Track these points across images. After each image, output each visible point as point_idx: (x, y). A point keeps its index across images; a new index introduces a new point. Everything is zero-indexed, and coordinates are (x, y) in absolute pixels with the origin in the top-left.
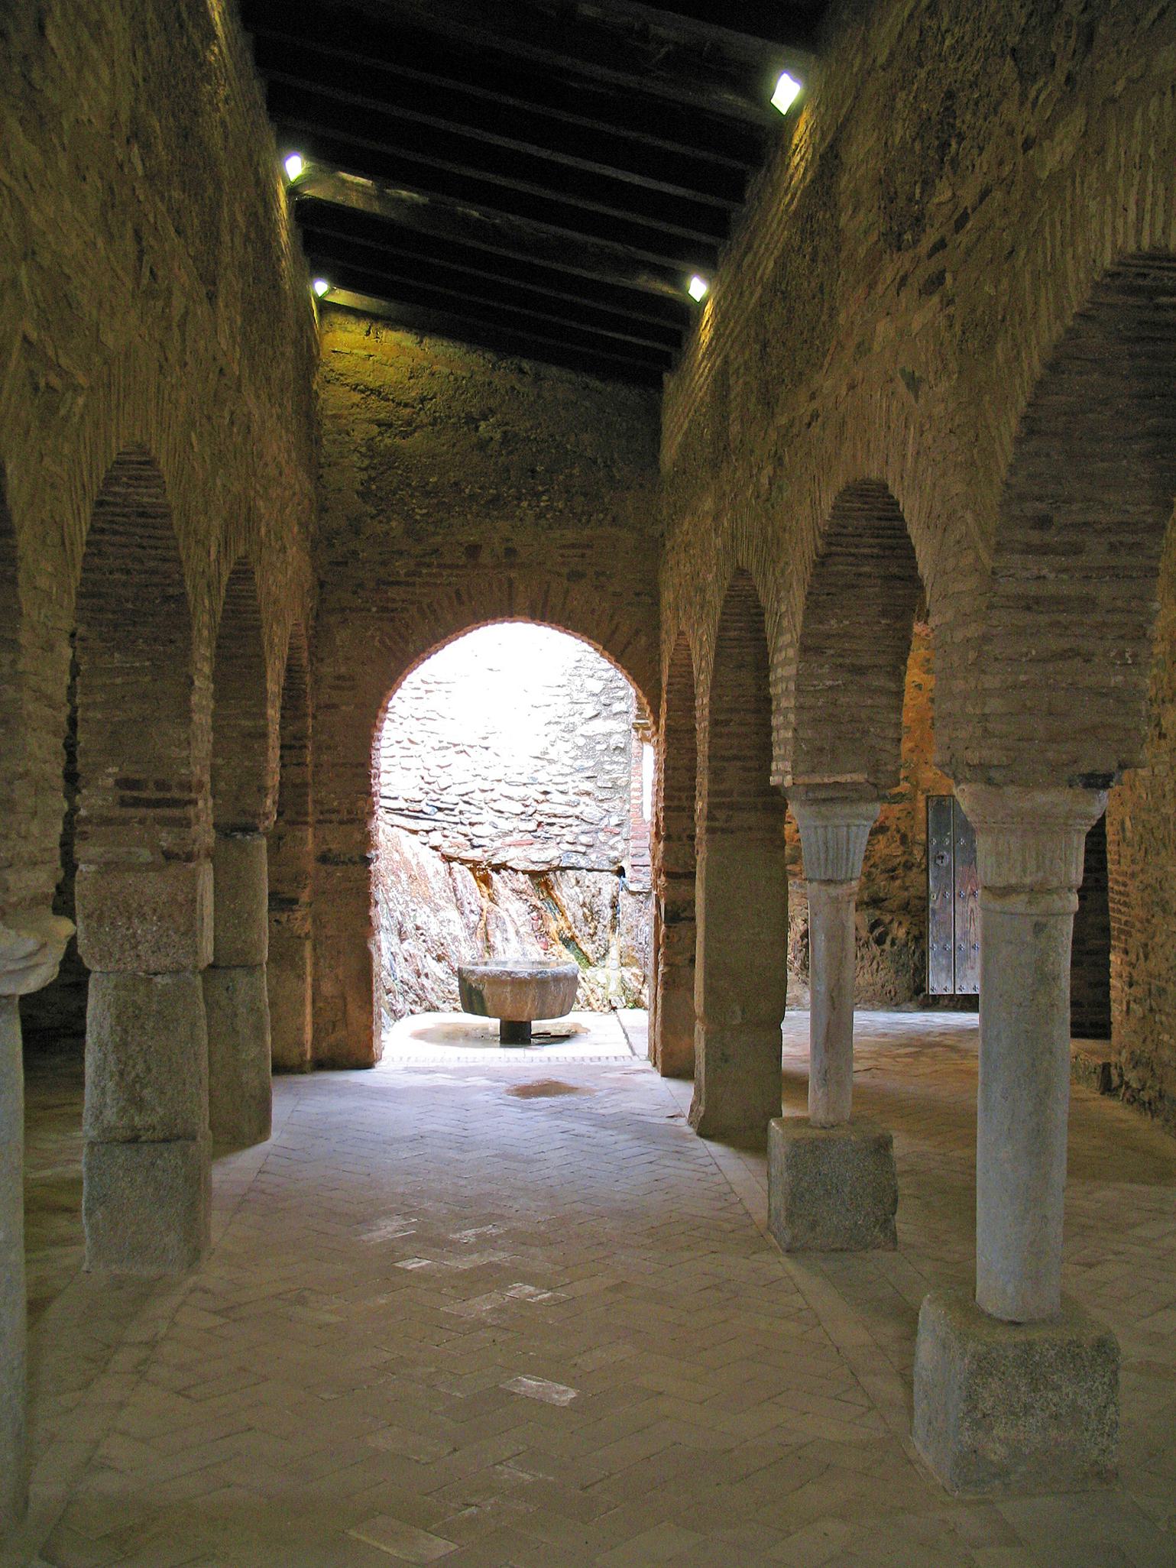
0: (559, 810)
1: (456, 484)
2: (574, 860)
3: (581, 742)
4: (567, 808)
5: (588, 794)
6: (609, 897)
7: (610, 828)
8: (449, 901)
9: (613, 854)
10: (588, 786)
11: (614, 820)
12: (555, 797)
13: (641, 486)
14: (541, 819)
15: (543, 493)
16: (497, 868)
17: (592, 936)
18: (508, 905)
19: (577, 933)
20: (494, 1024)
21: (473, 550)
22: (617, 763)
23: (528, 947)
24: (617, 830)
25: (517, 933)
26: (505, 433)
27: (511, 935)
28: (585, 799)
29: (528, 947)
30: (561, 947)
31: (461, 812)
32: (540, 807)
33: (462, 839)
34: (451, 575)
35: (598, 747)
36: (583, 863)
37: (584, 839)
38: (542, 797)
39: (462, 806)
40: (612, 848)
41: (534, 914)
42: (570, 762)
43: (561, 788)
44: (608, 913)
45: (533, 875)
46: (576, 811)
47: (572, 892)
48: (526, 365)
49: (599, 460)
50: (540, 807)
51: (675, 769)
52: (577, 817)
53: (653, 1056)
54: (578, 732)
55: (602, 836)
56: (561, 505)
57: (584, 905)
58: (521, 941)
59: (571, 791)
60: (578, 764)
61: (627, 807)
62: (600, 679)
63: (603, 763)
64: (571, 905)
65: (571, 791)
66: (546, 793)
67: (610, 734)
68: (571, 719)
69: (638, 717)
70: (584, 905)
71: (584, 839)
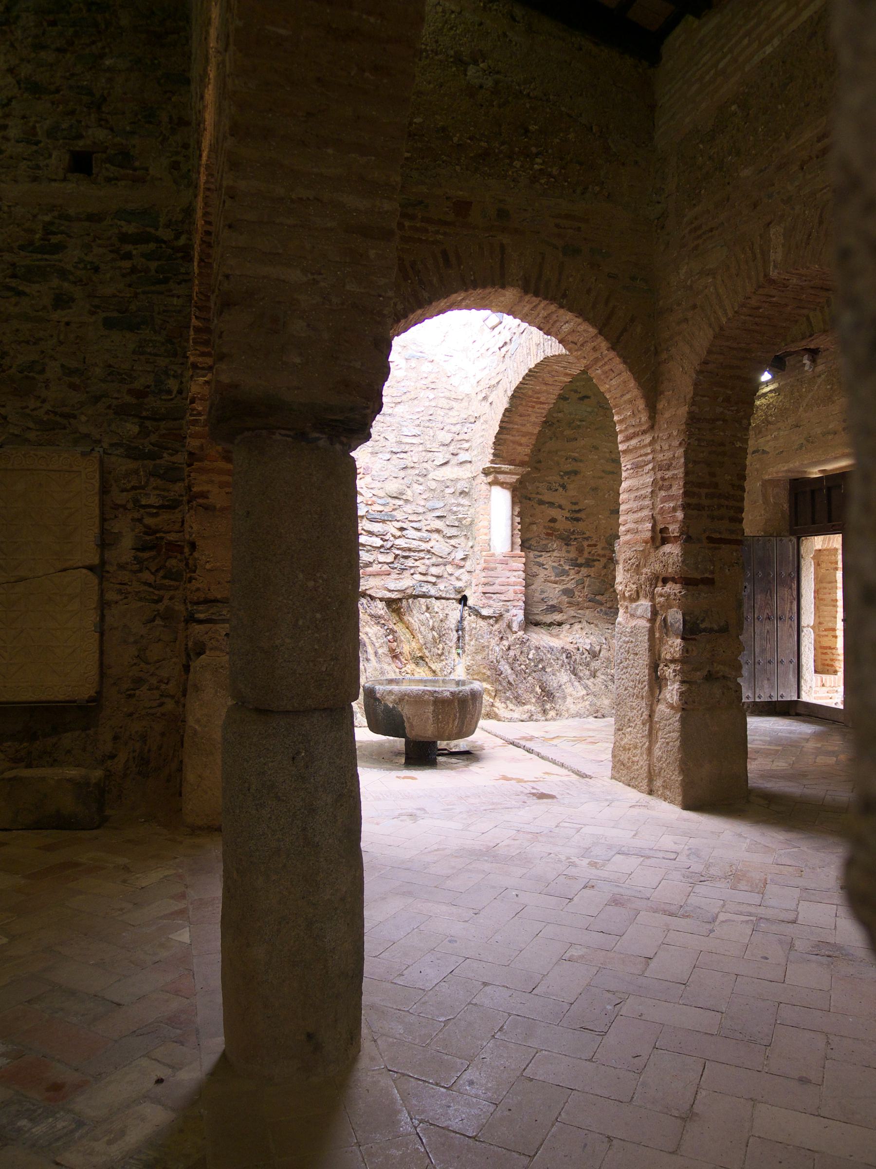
0: (414, 544)
1: (444, 129)
2: (425, 589)
4: (420, 543)
5: (438, 531)
6: (454, 622)
7: (456, 561)
9: (459, 584)
10: (439, 524)
11: (460, 555)
12: (411, 533)
13: (636, 162)
14: (397, 552)
15: (537, 155)
17: (440, 655)
18: (367, 629)
19: (427, 654)
20: (399, 743)
21: (462, 207)
23: (386, 666)
24: (462, 563)
25: (376, 653)
26: (497, 83)
28: (435, 536)
29: (386, 666)
30: (413, 666)
34: (437, 232)
35: (448, 491)
36: (433, 591)
37: (434, 570)
38: (398, 533)
40: (458, 579)
41: (390, 637)
42: (422, 503)
43: (415, 525)
44: (454, 635)
47: (422, 617)
48: (518, 12)
49: (595, 129)
51: (695, 462)
52: (429, 551)
53: (621, 768)
54: (430, 476)
55: (450, 569)
56: (555, 171)
57: (433, 629)
58: (379, 661)
60: (430, 504)
62: (449, 431)
64: (422, 628)
66: (402, 529)
67: (458, 480)
69: (492, 462)
70: (433, 629)
71: (434, 570)
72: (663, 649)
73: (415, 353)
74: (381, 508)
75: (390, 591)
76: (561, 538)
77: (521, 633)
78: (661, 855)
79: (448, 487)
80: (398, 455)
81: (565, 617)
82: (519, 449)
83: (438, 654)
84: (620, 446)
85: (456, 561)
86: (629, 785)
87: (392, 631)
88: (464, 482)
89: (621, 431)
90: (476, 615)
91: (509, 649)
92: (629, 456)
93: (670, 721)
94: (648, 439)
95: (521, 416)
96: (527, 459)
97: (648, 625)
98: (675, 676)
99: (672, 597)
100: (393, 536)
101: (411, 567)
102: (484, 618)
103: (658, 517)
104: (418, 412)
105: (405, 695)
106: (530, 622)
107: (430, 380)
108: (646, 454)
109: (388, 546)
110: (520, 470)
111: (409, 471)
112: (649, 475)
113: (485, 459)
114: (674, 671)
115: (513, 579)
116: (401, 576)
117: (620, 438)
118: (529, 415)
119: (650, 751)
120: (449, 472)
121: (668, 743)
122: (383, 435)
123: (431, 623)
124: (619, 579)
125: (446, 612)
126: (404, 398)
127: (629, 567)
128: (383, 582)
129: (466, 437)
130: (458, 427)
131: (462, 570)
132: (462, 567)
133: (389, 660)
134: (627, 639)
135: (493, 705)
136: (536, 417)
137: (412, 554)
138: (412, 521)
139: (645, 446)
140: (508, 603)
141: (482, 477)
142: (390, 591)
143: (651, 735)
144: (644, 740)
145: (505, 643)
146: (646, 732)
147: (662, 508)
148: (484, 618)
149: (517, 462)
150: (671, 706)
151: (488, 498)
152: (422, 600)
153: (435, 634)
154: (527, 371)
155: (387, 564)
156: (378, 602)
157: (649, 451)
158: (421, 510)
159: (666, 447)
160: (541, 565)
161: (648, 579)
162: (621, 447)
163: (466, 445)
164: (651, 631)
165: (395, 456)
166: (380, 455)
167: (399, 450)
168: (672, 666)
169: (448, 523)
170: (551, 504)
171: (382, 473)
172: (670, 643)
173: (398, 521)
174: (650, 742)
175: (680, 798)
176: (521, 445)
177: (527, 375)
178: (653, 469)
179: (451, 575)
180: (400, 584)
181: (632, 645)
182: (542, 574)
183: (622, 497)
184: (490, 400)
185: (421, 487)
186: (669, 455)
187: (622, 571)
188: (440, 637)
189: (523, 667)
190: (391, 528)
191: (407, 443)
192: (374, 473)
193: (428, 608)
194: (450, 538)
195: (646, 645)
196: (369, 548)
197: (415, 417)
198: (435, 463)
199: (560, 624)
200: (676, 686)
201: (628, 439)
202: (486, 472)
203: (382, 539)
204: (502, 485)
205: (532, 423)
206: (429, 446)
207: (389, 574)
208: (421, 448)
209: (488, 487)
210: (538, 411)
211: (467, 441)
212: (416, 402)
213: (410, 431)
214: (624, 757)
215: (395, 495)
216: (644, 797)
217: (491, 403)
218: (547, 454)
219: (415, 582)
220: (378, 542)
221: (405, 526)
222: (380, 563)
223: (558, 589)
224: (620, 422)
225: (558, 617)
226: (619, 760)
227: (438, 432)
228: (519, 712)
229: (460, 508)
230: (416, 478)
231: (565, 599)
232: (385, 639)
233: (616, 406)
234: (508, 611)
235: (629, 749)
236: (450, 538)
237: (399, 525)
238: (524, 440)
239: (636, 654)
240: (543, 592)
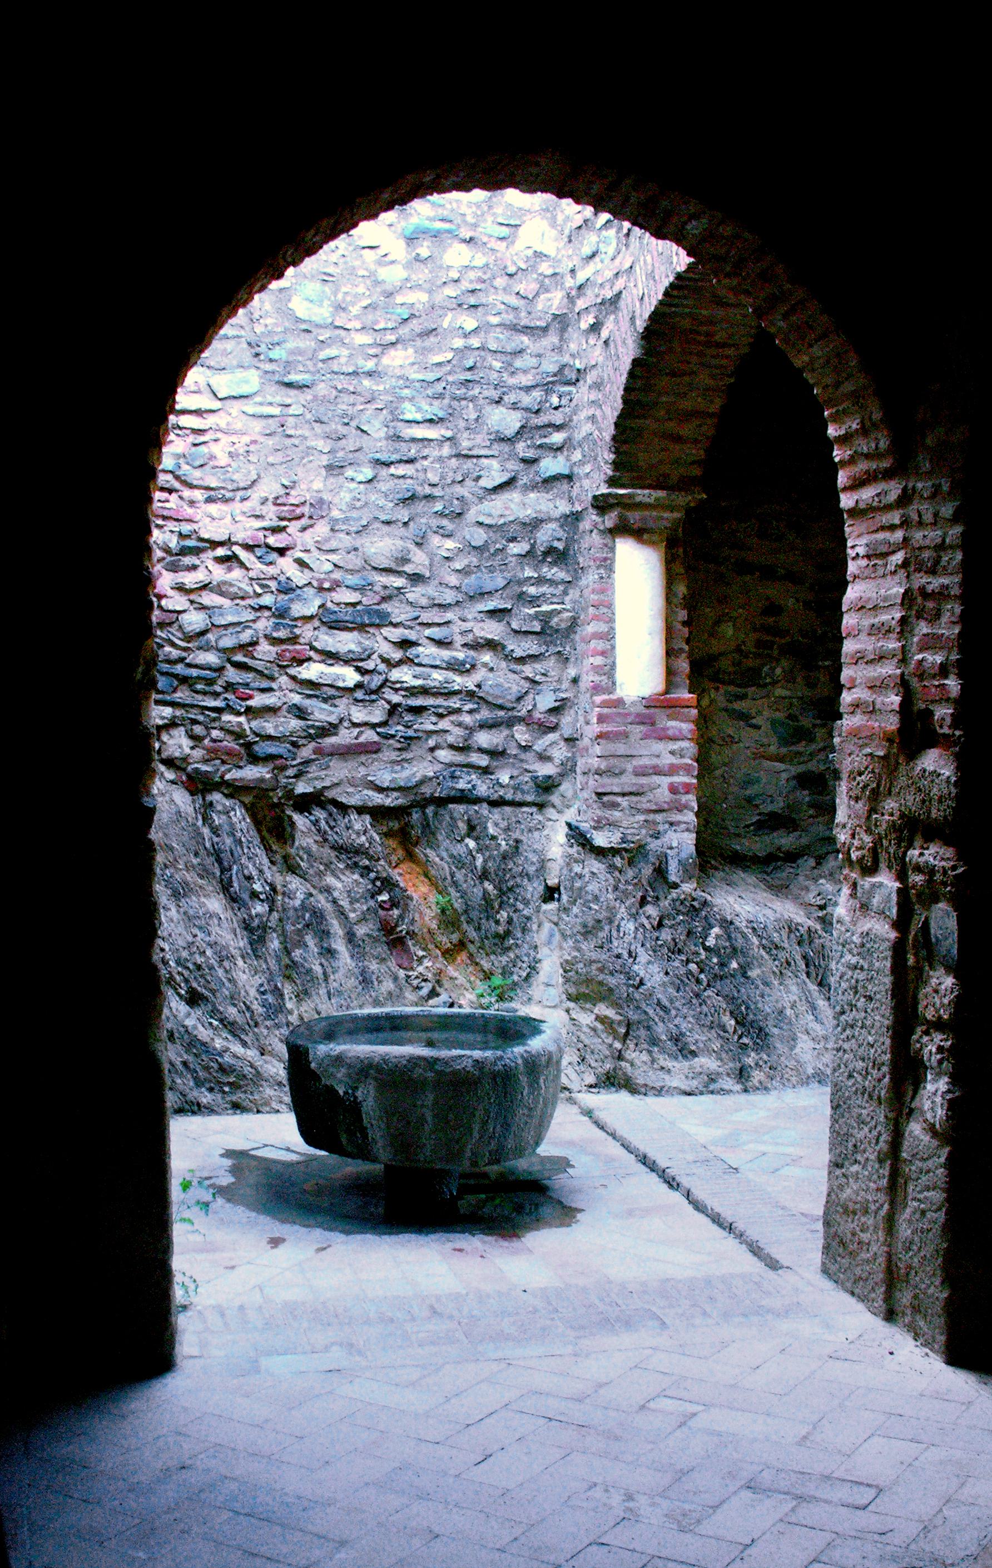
3: (479, 537)
4: (451, 675)
5: (491, 645)
7: (537, 715)
8: (204, 873)
10: (492, 630)
11: (546, 701)
12: (427, 652)
14: (396, 699)
16: (305, 803)
19: (473, 934)
22: (551, 582)
23: (374, 966)
25: (350, 937)
27: (340, 945)
28: (487, 657)
31: (229, 687)
32: (395, 674)
33: (230, 743)
36: (483, 789)
37: (484, 739)
38: (397, 655)
39: (232, 674)
40: (543, 757)
41: (384, 897)
42: (453, 580)
45: (378, 813)
46: (469, 682)
50: (395, 674)
52: (471, 694)
53: (838, 1251)
54: (472, 515)
55: (521, 734)
57: (484, 876)
59: (459, 641)
60: (470, 582)
61: (572, 672)
62: (515, 406)
63: (521, 582)
64: (459, 876)
65: (459, 641)
66: (405, 644)
67: (536, 524)
68: (459, 490)
69: (611, 482)
70: (484, 876)
71: (484, 739)
72: (921, 996)
73: (427, 224)
74: (352, 597)
75: (380, 790)
76: (791, 650)
77: (688, 887)
78: (843, 1493)
79: (513, 539)
80: (392, 470)
81: (804, 841)
82: (677, 450)
83: (497, 935)
84: (842, 496)
85: (537, 715)
86: (853, 1294)
87: (388, 884)
88: (553, 525)
89: (843, 463)
90: (583, 846)
91: (660, 925)
92: (861, 526)
93: (930, 1164)
94: (894, 490)
95: (673, 374)
96: (696, 471)
97: (893, 935)
98: (940, 1062)
99: (938, 877)
100: (385, 660)
101: (430, 733)
102: (600, 852)
103: (914, 682)
104: (439, 364)
105: (370, 1066)
106: (714, 856)
107: (465, 285)
108: (892, 528)
109: (373, 686)
110: (682, 499)
111: (420, 507)
112: (897, 578)
113: (594, 479)
114: (940, 1049)
115: (668, 760)
116: (408, 755)
117: (842, 478)
118: (692, 373)
119: (890, 1223)
120: (519, 506)
121: (923, 1213)
122: (353, 424)
123: (479, 861)
124: (841, 815)
125: (517, 835)
126: (404, 331)
127: (857, 792)
128: (363, 771)
129: (558, 418)
130: (537, 394)
131: (552, 737)
132: (554, 729)
133: (382, 949)
134: (854, 961)
135: (620, 1057)
136: (712, 376)
137: (429, 701)
138: (428, 625)
139: (888, 508)
140: (659, 817)
141: (592, 517)
142: (380, 790)
143: (895, 1186)
144: (882, 1197)
145: (651, 910)
146: (884, 1182)
147: (920, 662)
148: (600, 852)
149: (674, 479)
150: (931, 1129)
151: (607, 564)
152: (461, 808)
153: (489, 887)
154: (671, 279)
155: (373, 726)
156: (353, 816)
157: (897, 521)
158: (449, 597)
159: (928, 518)
160: (744, 717)
161: (893, 826)
162: (846, 501)
163: (557, 438)
164: (898, 949)
165: (384, 472)
166: (349, 473)
167: (394, 457)
168: (938, 1037)
169: (515, 625)
170: (768, 573)
171: (355, 514)
172: (934, 981)
173: (395, 625)
174: (892, 1203)
175: (943, 1338)
176: (678, 439)
177: (672, 285)
178: (905, 564)
179: (526, 748)
180: (406, 773)
181: (862, 976)
182: (748, 738)
183: (849, 621)
184: (605, 334)
185: (450, 544)
186: (934, 535)
187: (846, 800)
188: (502, 893)
189: (693, 967)
190: (381, 644)
191: (414, 440)
192: (335, 513)
193: (471, 828)
194: (521, 660)
195: (888, 980)
196: (332, 692)
197: (430, 376)
198: (482, 483)
199: (792, 857)
200: (942, 1084)
201: (857, 484)
202: (601, 504)
203: (358, 669)
204: (639, 534)
205: (703, 392)
206: (465, 444)
207: (377, 751)
208: (446, 450)
209: (608, 540)
210: (715, 362)
211: (559, 428)
212: (432, 339)
213: (419, 409)
214: (847, 1226)
215: (385, 564)
216: (878, 1324)
217: (606, 343)
218: (701, 501)
219: (438, 767)
220: (350, 676)
221: (412, 635)
222: (355, 725)
223: (784, 776)
224: (844, 440)
225: (786, 841)
226: (836, 1234)
227: (488, 409)
228: (679, 1072)
229: (544, 589)
230: (434, 522)
231: (805, 796)
232: (372, 903)
233: (831, 403)
234: (657, 836)
235: (854, 1213)
236: (521, 660)
237: (396, 634)
238: (686, 430)
239: (870, 998)
240: (748, 782)
